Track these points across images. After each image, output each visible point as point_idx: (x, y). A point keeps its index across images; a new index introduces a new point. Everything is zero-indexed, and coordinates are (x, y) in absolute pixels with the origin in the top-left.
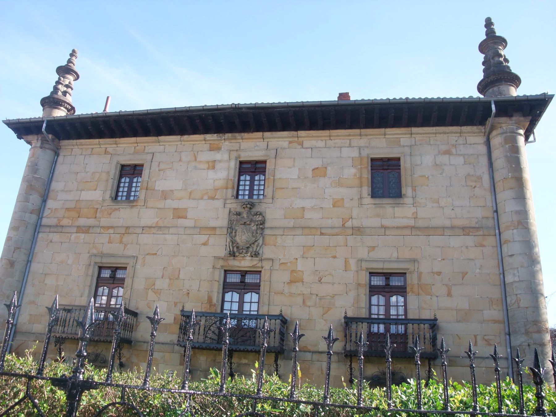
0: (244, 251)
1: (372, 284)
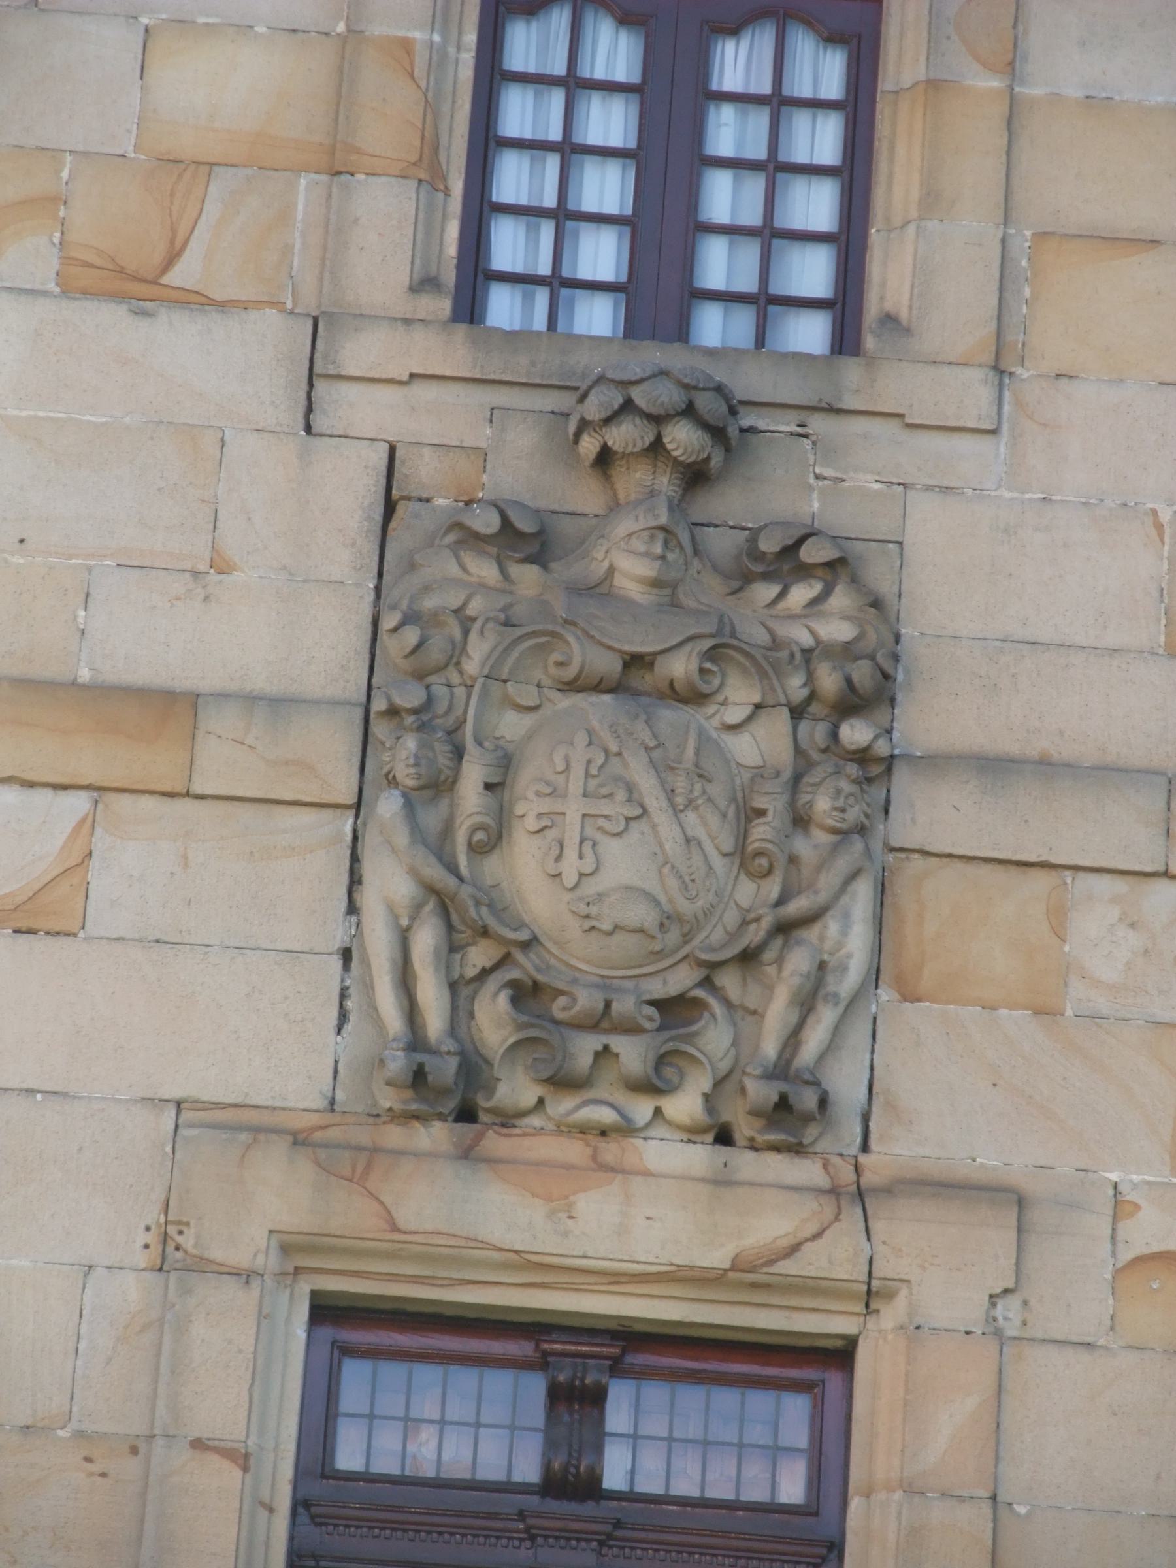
0: (632, 1054)
1: (348, 1458)
